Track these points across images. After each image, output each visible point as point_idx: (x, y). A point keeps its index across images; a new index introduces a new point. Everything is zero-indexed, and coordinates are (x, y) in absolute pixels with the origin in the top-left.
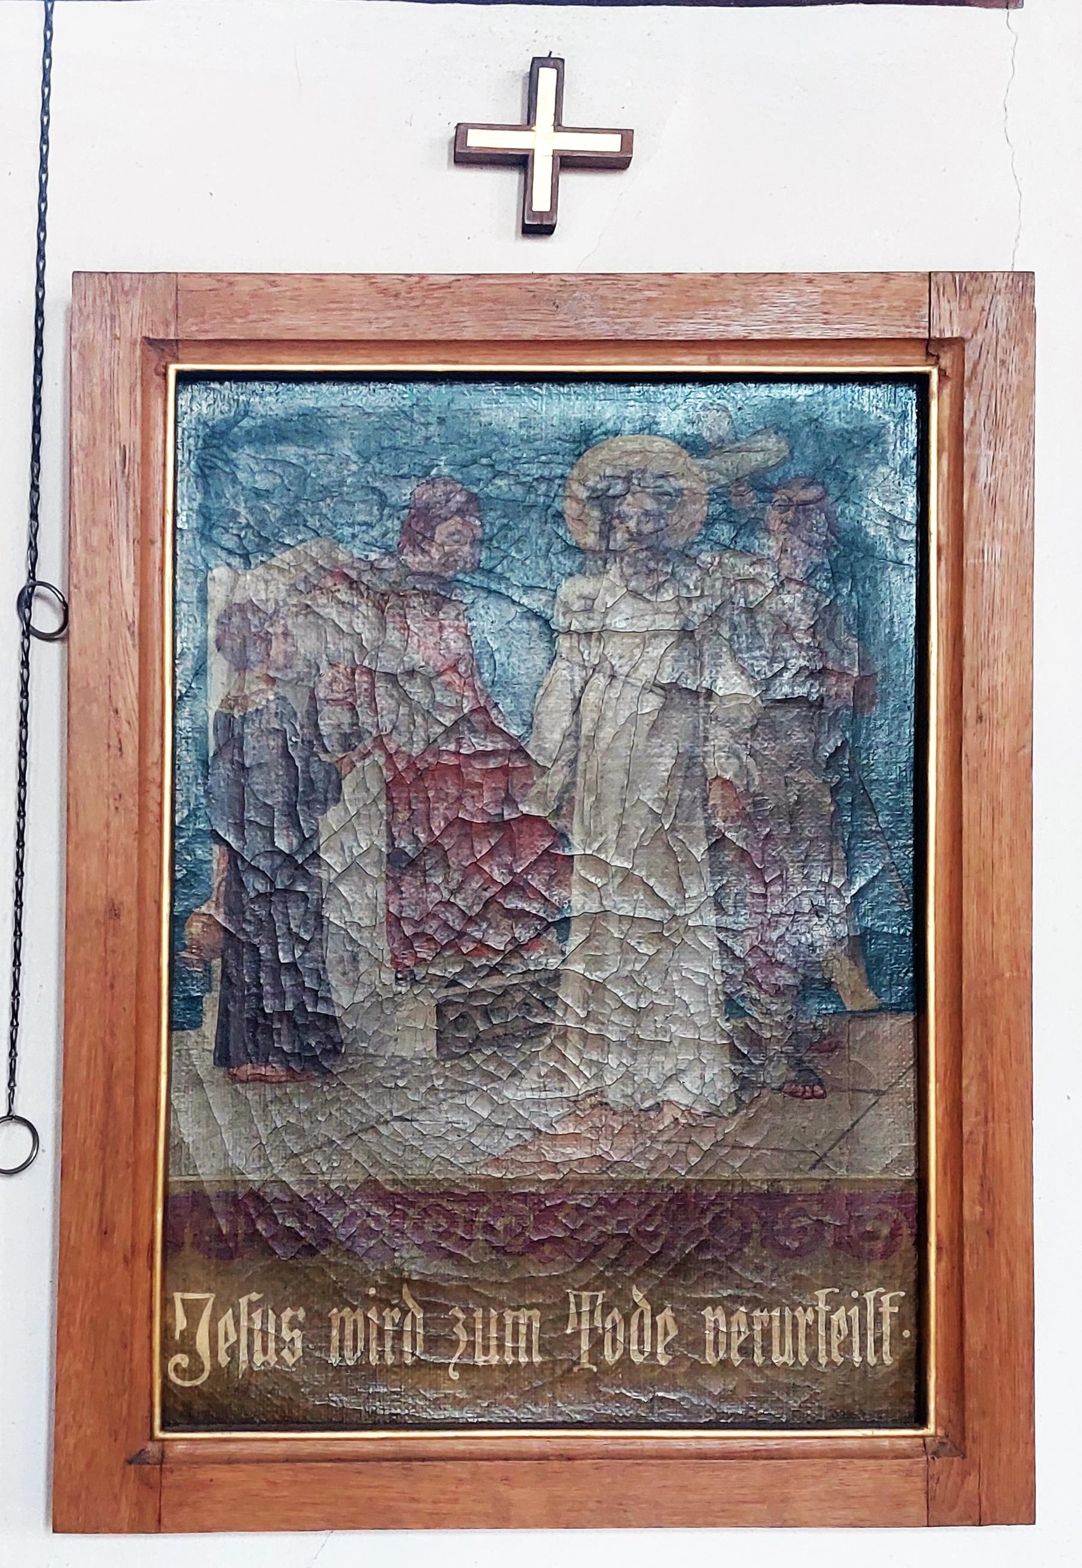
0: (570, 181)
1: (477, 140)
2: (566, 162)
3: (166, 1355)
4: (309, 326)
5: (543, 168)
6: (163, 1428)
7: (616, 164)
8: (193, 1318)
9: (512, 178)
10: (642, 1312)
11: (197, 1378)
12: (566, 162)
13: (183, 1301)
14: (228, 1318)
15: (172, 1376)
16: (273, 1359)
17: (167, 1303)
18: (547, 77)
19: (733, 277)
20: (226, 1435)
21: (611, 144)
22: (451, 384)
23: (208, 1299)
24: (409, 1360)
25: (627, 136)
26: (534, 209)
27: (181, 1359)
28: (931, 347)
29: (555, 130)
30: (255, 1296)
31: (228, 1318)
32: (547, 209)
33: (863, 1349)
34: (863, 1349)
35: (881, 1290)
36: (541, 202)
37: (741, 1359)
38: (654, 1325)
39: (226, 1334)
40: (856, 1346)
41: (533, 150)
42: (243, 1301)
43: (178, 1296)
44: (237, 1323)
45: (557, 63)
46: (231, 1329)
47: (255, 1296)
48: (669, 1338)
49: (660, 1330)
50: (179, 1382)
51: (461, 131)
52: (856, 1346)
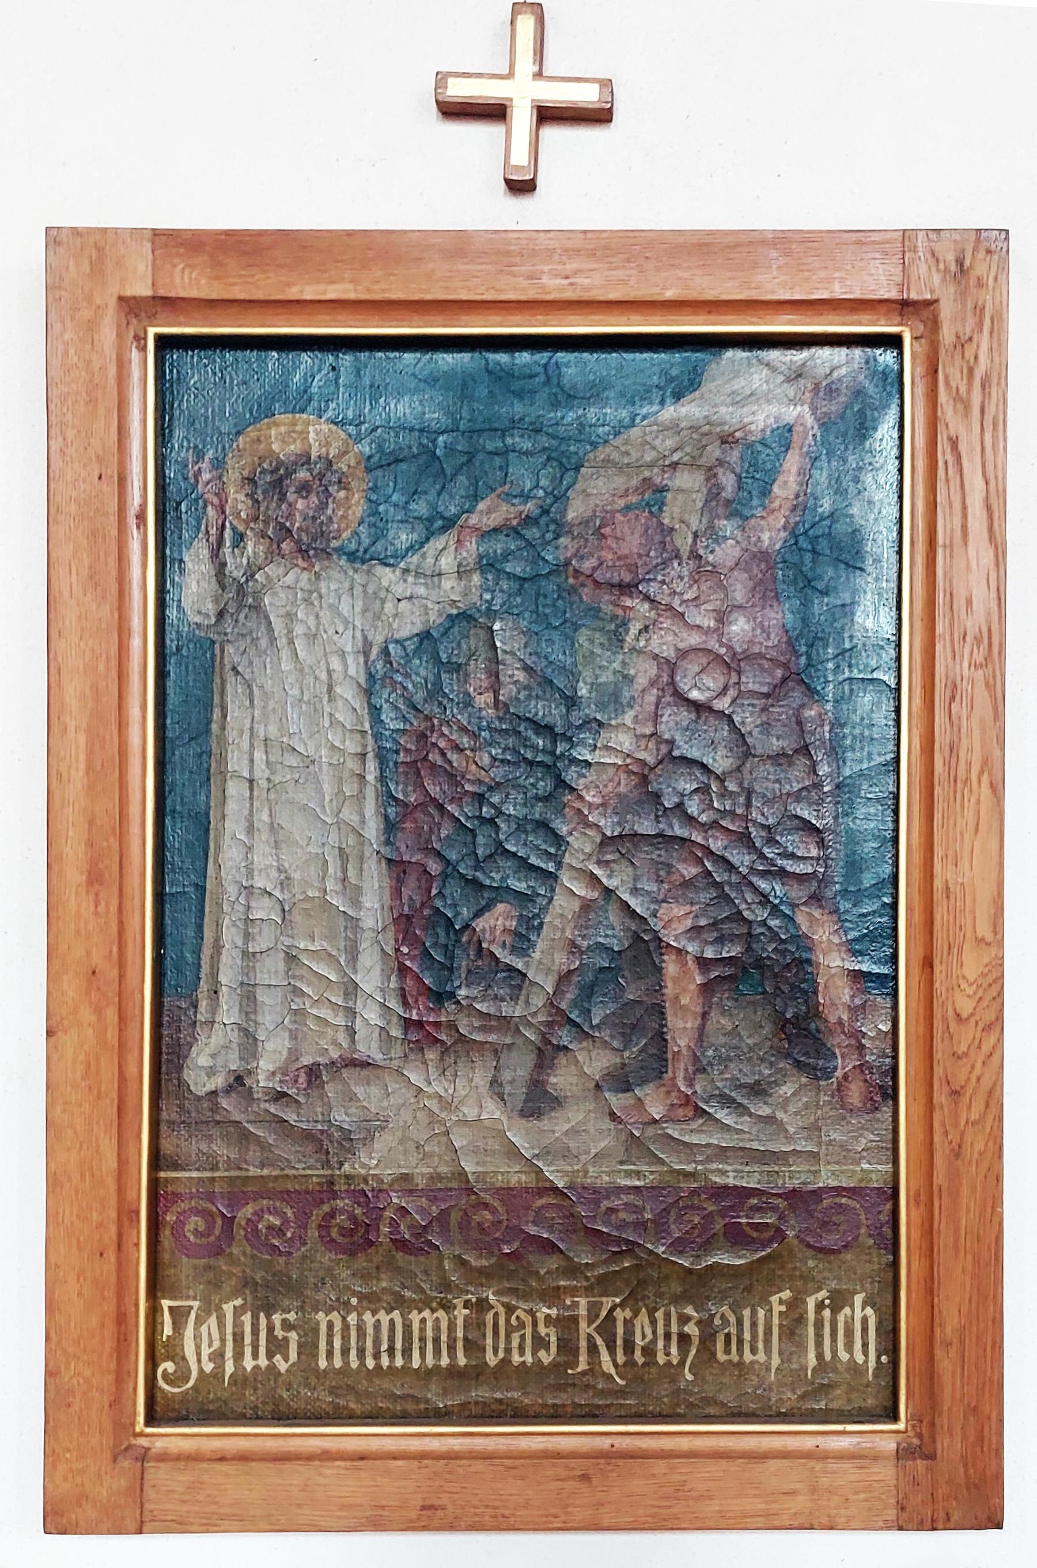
0: (552, 134)
1: (459, 90)
3: (152, 1361)
4: (554, 287)
5: (522, 118)
6: (895, 1418)
8: (178, 1326)
10: (496, 1314)
11: (187, 1382)
13: (170, 1308)
14: (213, 1320)
15: (161, 1382)
16: (529, 1359)
17: (154, 1312)
19: (582, 236)
20: (850, 1428)
21: (587, 95)
22: (802, 349)
23: (191, 1308)
24: (492, 1360)
25: (606, 84)
27: (169, 1366)
28: (904, 307)
30: (239, 1302)
31: (213, 1320)
34: (330, 1354)
37: (643, 1359)
38: (197, 1337)
40: (229, 1354)
41: (511, 100)
43: (166, 1303)
47: (239, 1302)
50: (176, 1390)
51: (441, 79)
52: (229, 1354)
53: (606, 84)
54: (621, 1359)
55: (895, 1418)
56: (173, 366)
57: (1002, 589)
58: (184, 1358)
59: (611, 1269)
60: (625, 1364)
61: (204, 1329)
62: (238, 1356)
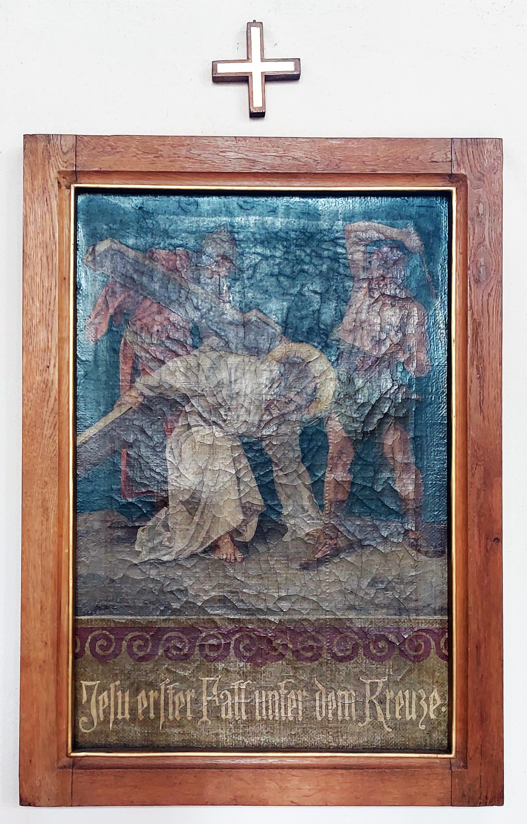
0: (271, 87)
1: (223, 69)
2: (269, 79)
5: (257, 81)
6: (450, 752)
7: (294, 78)
9: (241, 89)
12: (269, 79)
14: (105, 693)
17: (76, 690)
18: (255, 31)
21: (288, 68)
25: (297, 61)
26: (294, 70)
27: (84, 719)
29: (262, 61)
32: (261, 106)
33: (411, 697)
35: (242, 681)
36: (257, 103)
38: (97, 702)
39: (142, 704)
42: (112, 686)
43: (84, 683)
44: (109, 697)
45: (260, 25)
46: (106, 700)
48: (105, 706)
49: (101, 703)
53: (297, 61)
54: (388, 716)
55: (450, 752)
56: (439, 371)
57: (251, 97)
58: (91, 715)
59: (89, 640)
60: (391, 719)
61: (100, 698)
62: (116, 714)
